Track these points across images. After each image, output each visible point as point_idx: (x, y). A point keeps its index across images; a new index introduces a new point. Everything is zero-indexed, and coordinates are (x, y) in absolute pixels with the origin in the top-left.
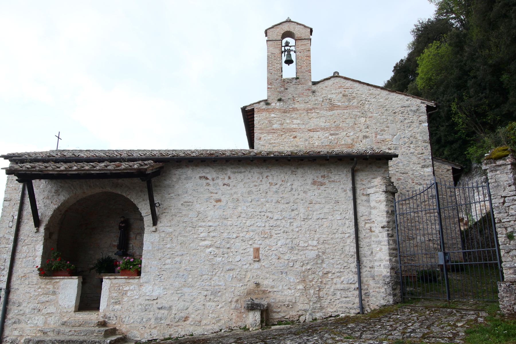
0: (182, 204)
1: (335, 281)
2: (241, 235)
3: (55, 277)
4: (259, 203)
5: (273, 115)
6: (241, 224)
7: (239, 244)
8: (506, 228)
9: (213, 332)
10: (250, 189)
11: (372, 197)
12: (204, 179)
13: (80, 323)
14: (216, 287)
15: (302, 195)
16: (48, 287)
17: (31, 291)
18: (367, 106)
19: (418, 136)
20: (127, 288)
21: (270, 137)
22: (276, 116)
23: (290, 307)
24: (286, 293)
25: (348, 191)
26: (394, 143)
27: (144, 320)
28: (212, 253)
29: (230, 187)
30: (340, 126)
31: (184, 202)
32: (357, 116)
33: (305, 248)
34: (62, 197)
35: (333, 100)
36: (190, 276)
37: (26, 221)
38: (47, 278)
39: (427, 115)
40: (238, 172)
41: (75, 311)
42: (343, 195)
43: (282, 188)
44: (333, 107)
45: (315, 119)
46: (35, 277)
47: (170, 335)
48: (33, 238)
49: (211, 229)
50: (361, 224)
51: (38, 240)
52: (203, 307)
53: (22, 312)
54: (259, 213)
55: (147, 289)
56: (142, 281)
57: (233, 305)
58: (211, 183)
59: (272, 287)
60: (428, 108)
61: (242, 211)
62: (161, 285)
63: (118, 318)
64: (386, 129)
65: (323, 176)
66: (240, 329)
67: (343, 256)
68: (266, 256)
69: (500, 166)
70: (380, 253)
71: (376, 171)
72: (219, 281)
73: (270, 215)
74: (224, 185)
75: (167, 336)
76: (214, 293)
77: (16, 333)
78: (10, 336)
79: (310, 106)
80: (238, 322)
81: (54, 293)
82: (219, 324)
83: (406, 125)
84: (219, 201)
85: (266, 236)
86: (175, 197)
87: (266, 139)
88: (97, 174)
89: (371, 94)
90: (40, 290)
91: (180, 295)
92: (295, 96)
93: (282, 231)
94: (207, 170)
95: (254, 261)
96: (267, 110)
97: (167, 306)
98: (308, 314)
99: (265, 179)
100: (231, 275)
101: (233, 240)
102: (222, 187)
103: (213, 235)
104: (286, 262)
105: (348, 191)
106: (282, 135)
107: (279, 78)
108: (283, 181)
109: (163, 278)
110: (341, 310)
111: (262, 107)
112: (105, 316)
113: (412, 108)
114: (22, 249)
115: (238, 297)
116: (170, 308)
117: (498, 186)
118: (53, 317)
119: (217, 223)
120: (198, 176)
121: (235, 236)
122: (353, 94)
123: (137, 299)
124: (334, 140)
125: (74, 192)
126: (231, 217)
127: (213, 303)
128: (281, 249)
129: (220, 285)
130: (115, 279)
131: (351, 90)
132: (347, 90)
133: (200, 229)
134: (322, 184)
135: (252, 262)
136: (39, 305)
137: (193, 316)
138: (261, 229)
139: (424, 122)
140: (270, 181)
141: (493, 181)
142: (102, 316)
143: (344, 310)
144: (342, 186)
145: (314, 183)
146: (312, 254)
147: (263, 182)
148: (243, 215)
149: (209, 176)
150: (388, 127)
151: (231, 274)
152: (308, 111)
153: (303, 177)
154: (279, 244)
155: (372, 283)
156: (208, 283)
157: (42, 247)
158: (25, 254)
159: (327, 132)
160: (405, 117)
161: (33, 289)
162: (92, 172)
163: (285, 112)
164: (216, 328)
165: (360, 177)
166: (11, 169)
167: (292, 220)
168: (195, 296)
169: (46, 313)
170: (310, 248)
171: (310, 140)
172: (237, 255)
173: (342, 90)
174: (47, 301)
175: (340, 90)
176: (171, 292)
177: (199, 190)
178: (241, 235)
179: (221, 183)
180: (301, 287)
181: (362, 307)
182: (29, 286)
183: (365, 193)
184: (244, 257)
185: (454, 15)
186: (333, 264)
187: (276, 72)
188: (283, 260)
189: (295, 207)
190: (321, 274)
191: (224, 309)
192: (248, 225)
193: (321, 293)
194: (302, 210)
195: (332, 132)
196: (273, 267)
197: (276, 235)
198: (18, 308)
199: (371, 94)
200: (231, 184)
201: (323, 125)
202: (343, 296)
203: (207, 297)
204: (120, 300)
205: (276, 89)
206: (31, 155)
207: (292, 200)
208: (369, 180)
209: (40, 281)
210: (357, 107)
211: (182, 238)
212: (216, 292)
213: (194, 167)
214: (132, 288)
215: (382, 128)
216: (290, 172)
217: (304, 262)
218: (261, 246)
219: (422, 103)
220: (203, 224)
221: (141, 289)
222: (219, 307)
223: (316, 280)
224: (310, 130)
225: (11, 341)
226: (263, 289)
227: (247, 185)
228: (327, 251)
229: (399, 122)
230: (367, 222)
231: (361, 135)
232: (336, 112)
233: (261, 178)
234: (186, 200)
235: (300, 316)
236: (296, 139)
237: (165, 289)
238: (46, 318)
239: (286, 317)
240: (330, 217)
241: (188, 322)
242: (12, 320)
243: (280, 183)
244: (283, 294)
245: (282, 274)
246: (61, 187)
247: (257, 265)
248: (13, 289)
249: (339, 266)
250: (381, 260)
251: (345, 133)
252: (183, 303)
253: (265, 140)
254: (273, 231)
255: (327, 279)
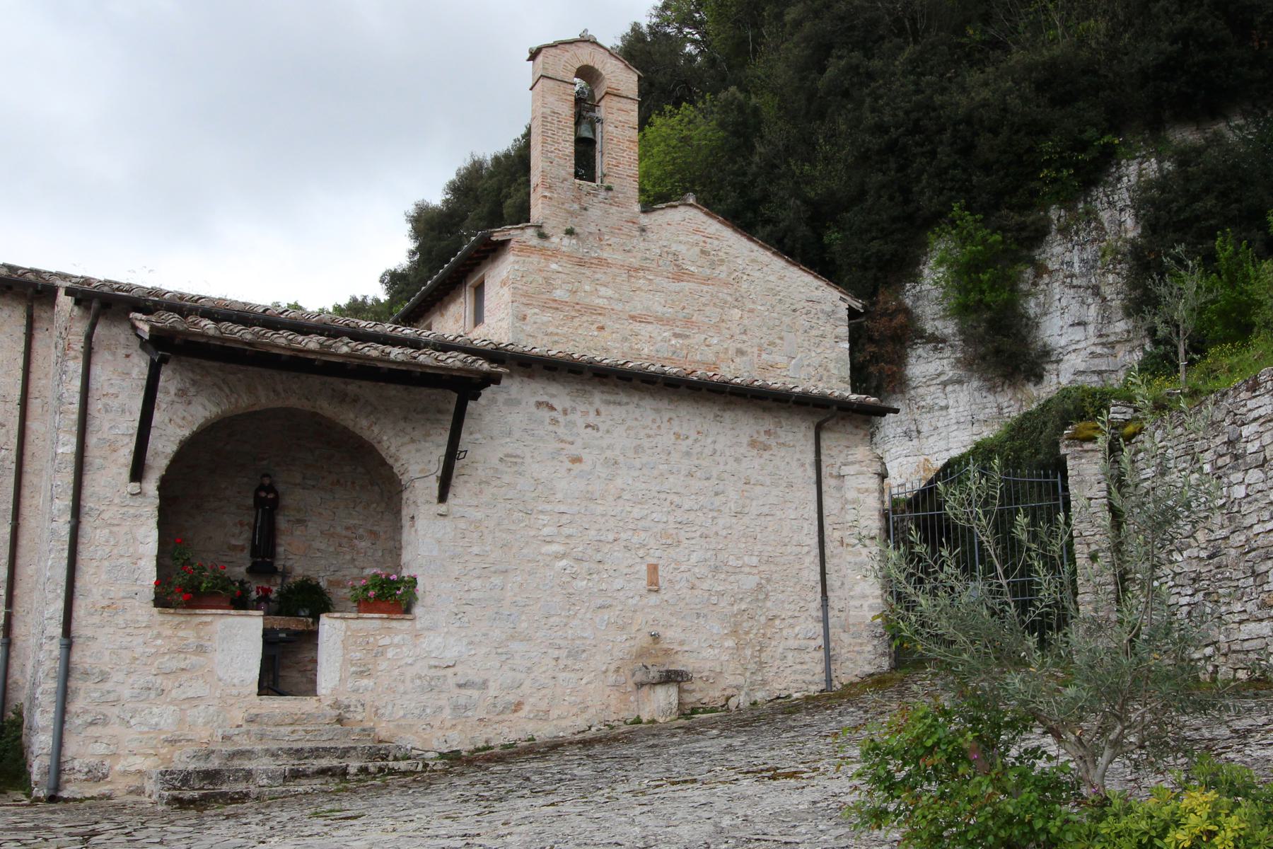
0: (501, 460)
1: (785, 633)
2: (623, 536)
3: (203, 611)
4: (656, 472)
5: (554, 266)
6: (624, 514)
7: (620, 555)
8: (1088, 545)
9: (575, 731)
10: (638, 442)
11: (851, 482)
12: (546, 409)
13: (296, 717)
14: (577, 642)
15: (732, 465)
16: (181, 633)
17: (135, 643)
18: (745, 285)
19: (831, 366)
20: (386, 641)
21: (546, 317)
22: (560, 269)
23: (711, 681)
24: (704, 654)
25: (807, 466)
26: (791, 374)
27: (428, 711)
28: (567, 572)
29: (600, 434)
30: (694, 319)
31: (508, 455)
32: (725, 303)
33: (738, 570)
34: (200, 408)
35: (680, 257)
36: (523, 617)
37: (98, 462)
38: (181, 611)
39: (849, 326)
40: (614, 403)
41: (259, 694)
42: (799, 472)
43: (697, 448)
44: (680, 274)
45: (643, 294)
46: (144, 610)
47: (486, 742)
48: (126, 509)
49: (564, 519)
50: (828, 530)
51: (141, 516)
52: (552, 683)
53: (112, 697)
54: (656, 494)
55: (433, 643)
56: (418, 625)
57: (612, 678)
58: (561, 419)
59: (682, 643)
60: (852, 313)
61: (625, 486)
62: (463, 634)
63: (368, 709)
64: (778, 341)
65: (768, 432)
66: (625, 722)
67: (798, 588)
68: (670, 581)
69: (1087, 451)
70: (862, 584)
71: (851, 433)
72: (584, 629)
73: (676, 499)
74: (586, 427)
75: (481, 745)
76: (574, 654)
77: (100, 749)
78: (82, 756)
79: (635, 262)
80: (621, 710)
81: (201, 650)
82: (586, 716)
83: (812, 341)
84: (577, 460)
85: (669, 541)
86: (484, 441)
87: (538, 321)
88: (390, 370)
89: (753, 261)
90: (159, 642)
91: (504, 657)
92: (603, 230)
93: (698, 533)
94: (554, 389)
95: (650, 590)
96: (542, 251)
97: (477, 680)
98: (743, 693)
99: (665, 425)
100: (606, 617)
101: (609, 546)
102: (582, 431)
103: (568, 532)
104: (706, 595)
105: (807, 466)
106: (573, 317)
107: (568, 176)
108: (699, 433)
109: (465, 619)
110: (795, 685)
111: (530, 240)
112: (336, 705)
113: (824, 307)
114: (94, 535)
115: (620, 662)
116: (484, 685)
117: (1082, 481)
118: (202, 707)
119: (576, 509)
120: (533, 400)
121: (611, 537)
122: (720, 254)
123: (411, 665)
124: (681, 349)
125: (233, 400)
126: (603, 497)
127: (572, 675)
128: (697, 570)
129: (585, 638)
130: (357, 618)
131: (716, 242)
132: (709, 240)
133: (541, 517)
134: (766, 448)
135: (644, 592)
136: (159, 680)
137: (532, 700)
138: (661, 526)
139: (843, 340)
140: (676, 429)
141: (1075, 473)
142: (329, 703)
143: (799, 686)
144: (798, 456)
145: (753, 444)
146: (750, 582)
147: (663, 430)
148: (626, 496)
149: (555, 402)
150: (781, 338)
151: (606, 615)
152: (632, 271)
153: (733, 429)
154: (694, 557)
155: (846, 638)
156: (560, 633)
157: (155, 534)
158: (107, 550)
159: (668, 327)
160: (813, 324)
161: (140, 640)
162: (380, 365)
163: (581, 263)
164: (581, 723)
165: (828, 440)
166: (175, 327)
167: (715, 514)
168: (535, 660)
169: (184, 696)
170: (747, 570)
171: (633, 339)
172: (616, 578)
173: (698, 238)
174: (183, 669)
175: (696, 237)
176: (484, 650)
177: (536, 432)
178: (623, 536)
179: (581, 422)
180: (730, 643)
181: (829, 680)
182: (128, 630)
183: (835, 473)
184: (629, 581)
185: (697, 36)
186: (783, 602)
187: (562, 162)
188: (701, 592)
189: (721, 487)
190: (763, 619)
191: (593, 686)
192: (636, 516)
193: (764, 655)
194: (733, 495)
195: (677, 330)
196: (682, 604)
197: (687, 541)
198: (99, 686)
199: (753, 261)
200: (603, 427)
201: (660, 309)
202: (798, 661)
203: (560, 661)
204: (370, 667)
205: (563, 204)
206: (43, 275)
207: (715, 474)
208: (840, 448)
209: (160, 618)
210: (727, 284)
211: (504, 535)
212: (577, 652)
213: (525, 379)
214: (397, 639)
215: (771, 339)
216: (712, 416)
217: (737, 597)
218: (661, 562)
219: (841, 299)
220: (548, 507)
221: (418, 642)
222: (584, 681)
223: (754, 631)
224: (633, 317)
225: (86, 770)
226: (666, 646)
227: (632, 433)
228: (775, 576)
229: (801, 331)
230: (835, 526)
231: (732, 346)
232: (687, 286)
233: (658, 420)
234: (509, 450)
235: (728, 699)
236: (604, 334)
237: (471, 643)
238: (181, 709)
239: (703, 701)
240: (779, 513)
241: (522, 714)
242: (86, 717)
243: (693, 435)
244: (701, 656)
245: (698, 618)
246: (194, 383)
247: (653, 599)
248: (79, 637)
249: (792, 606)
250: (864, 597)
251: (703, 336)
252: (511, 674)
253: (535, 323)
254: (682, 531)
255: (774, 630)
